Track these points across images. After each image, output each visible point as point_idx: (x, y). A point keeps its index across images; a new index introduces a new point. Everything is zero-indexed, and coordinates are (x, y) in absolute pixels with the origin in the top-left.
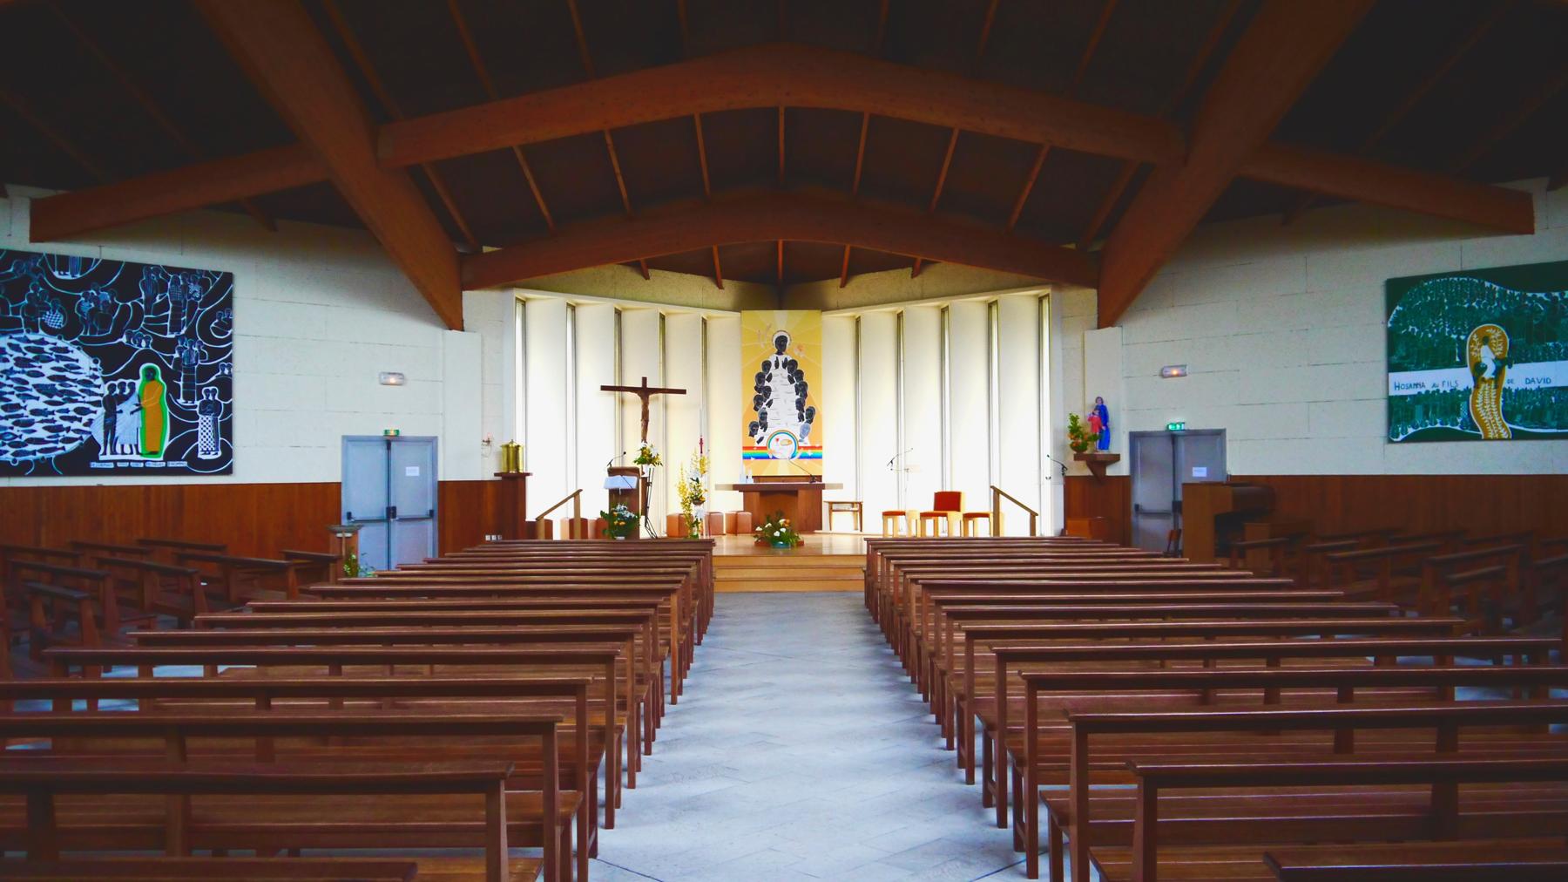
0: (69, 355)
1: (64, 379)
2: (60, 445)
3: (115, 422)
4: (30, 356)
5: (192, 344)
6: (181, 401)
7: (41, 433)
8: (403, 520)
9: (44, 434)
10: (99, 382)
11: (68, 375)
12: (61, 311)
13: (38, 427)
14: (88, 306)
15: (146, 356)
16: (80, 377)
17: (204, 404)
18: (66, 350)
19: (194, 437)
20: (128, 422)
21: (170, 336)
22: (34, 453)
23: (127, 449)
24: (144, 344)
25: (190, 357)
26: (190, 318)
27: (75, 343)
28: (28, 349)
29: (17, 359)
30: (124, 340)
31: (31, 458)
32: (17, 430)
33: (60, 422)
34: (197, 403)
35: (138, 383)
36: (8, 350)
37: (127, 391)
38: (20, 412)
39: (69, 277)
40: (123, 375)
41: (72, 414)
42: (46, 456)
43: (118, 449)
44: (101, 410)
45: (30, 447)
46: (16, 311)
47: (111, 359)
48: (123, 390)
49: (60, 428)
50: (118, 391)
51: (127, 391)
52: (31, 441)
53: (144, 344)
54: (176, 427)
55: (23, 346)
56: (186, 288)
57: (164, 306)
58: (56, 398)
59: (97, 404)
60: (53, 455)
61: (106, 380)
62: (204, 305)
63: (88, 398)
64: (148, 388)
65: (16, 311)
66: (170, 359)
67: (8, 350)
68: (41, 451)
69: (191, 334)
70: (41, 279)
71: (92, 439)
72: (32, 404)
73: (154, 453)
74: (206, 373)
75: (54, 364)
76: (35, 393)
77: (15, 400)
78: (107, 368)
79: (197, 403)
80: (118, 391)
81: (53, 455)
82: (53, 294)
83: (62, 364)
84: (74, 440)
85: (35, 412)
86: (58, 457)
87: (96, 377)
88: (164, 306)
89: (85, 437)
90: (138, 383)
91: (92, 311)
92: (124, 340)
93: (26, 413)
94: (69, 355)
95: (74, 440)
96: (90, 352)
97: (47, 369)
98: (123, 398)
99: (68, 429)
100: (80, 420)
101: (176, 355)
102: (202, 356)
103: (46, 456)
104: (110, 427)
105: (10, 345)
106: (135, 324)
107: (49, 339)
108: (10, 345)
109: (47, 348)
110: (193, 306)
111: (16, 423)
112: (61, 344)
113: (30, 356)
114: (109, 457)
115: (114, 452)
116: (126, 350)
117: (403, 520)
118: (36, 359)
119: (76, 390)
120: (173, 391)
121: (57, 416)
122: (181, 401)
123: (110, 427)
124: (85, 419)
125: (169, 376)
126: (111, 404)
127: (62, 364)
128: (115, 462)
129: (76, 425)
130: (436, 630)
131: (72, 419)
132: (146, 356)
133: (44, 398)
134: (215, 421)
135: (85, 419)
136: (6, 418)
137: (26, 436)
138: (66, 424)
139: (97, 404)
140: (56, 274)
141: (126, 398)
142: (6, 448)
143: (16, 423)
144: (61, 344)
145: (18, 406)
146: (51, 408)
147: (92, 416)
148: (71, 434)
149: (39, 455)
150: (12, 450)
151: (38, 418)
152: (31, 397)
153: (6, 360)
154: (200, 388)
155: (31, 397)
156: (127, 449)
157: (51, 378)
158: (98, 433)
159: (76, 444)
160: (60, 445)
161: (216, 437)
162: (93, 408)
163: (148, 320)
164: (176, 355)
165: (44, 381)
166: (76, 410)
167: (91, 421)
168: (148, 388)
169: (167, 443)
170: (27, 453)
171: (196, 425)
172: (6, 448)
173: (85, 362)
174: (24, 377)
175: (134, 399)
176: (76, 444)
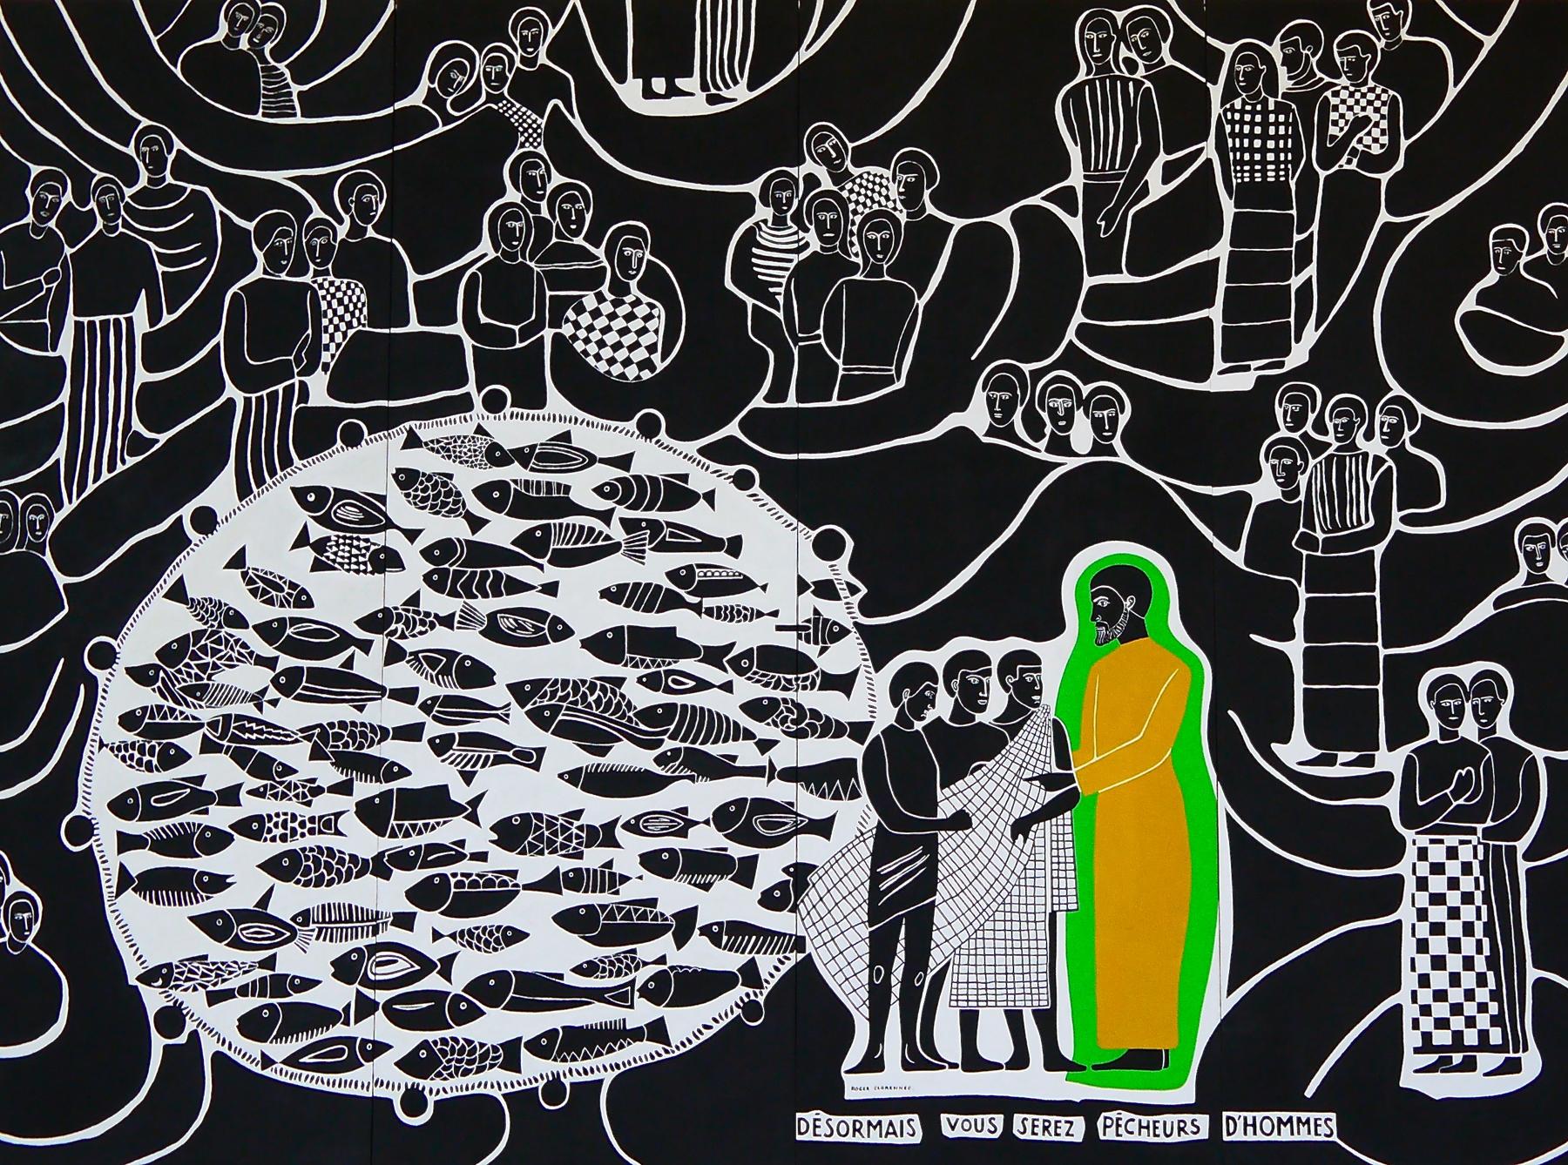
0: (695, 517)
1: (668, 644)
2: (642, 1013)
3: (927, 882)
4: (503, 530)
5: (1351, 418)
6: (1296, 750)
7: (554, 952)
8: (1063, 759)
9: (554, 952)
10: (847, 655)
11: (686, 624)
12: (654, 284)
13: (531, 911)
14: (781, 247)
15: (1098, 503)
16: (747, 636)
17: (1434, 766)
18: (678, 494)
19: (1377, 962)
20: (994, 876)
21: (1224, 381)
22: (510, 1055)
23: (994, 1041)
24: (1082, 435)
25: (1339, 497)
26: (1331, 280)
27: (721, 452)
28: (490, 494)
29: (440, 551)
30: (975, 417)
31: (495, 1082)
32: (431, 931)
33: (642, 885)
34: (1390, 761)
35: (1054, 655)
36: (400, 508)
37: (997, 701)
38: (447, 832)
39: (693, 105)
40: (969, 614)
41: (706, 839)
42: (572, 1071)
43: (947, 1039)
44: (856, 816)
45: (496, 1026)
46: (436, 302)
47: (928, 535)
48: (971, 697)
49: (634, 926)
50: (943, 706)
51: (997, 701)
52: (491, 990)
53: (1082, 435)
54: (1270, 907)
55: (467, 479)
56: (1309, 103)
57: (1189, 215)
58: (626, 756)
59: (828, 778)
60: (604, 1068)
61: (880, 646)
62: (1408, 196)
63: (789, 753)
64: (1119, 689)
65: (436, 302)
66: (1226, 515)
67: (400, 508)
68: (542, 1046)
69: (1342, 363)
70: (558, 131)
71: (805, 981)
72: (507, 792)
73: (1145, 1060)
74: (1434, 582)
75: (617, 569)
76: (520, 730)
77: (424, 768)
78: (886, 580)
79: (1390, 761)
80: (943, 706)
81: (604, 1068)
82: (617, 199)
83: (656, 568)
84: (696, 987)
85: (512, 833)
86: (628, 1081)
87: (830, 633)
88: (1189, 215)
89: (772, 967)
90: (1054, 655)
91: (814, 275)
92: (975, 417)
93: (479, 837)
94: (695, 517)
95: (696, 987)
96: (799, 494)
97: (582, 598)
98: (969, 746)
99: (684, 924)
100: (745, 873)
101: (1264, 490)
102: (1417, 484)
103: (572, 1071)
104: (902, 917)
105: (406, 479)
106: (1034, 331)
107: (604, 437)
108: (406, 479)
109: (582, 486)
110: (1351, 201)
111: (425, 896)
112: (658, 458)
113: (503, 530)
114: (895, 1080)
115: (920, 1057)
116: (993, 474)
117: (1063, 759)
118: (533, 544)
119: (727, 706)
120: (1250, 693)
121: (628, 854)
122: (1296, 750)
123: (902, 917)
124: (772, 866)
125: (1227, 615)
126: (909, 777)
127: (656, 568)
128: (930, 1109)
129: (726, 901)
130: (899, 875)
131: (703, 866)
132: (1098, 503)
133: (566, 754)
134: (1497, 867)
135: (772, 866)
136: (381, 867)
137: (472, 965)
138: (673, 895)
139: (828, 778)
140: (630, 92)
141: (989, 743)
142: (377, 1027)
143: (425, 896)
144: (658, 458)
145: (436, 803)
146: (598, 810)
147: (808, 848)
148: (700, 955)
149: (535, 1069)
150: (405, 1041)
151: (533, 867)
152: (500, 751)
153: (387, 561)
154: (1404, 674)
155: (500, 751)
156: (994, 1041)
157: (604, 645)
158: (846, 974)
159: (723, 1007)
160: (642, 1013)
161: (1504, 962)
162: (812, 805)
163: (1102, 302)
164: (1264, 490)
165: (568, 662)
166: (723, 818)
167: (801, 873)
168: (1119, 689)
169: (1217, 1004)
170: (476, 1057)
171: (1390, 893)
172: (377, 1027)
173: (776, 551)
174: (470, 643)
175: (1030, 749)
176: (723, 1007)
